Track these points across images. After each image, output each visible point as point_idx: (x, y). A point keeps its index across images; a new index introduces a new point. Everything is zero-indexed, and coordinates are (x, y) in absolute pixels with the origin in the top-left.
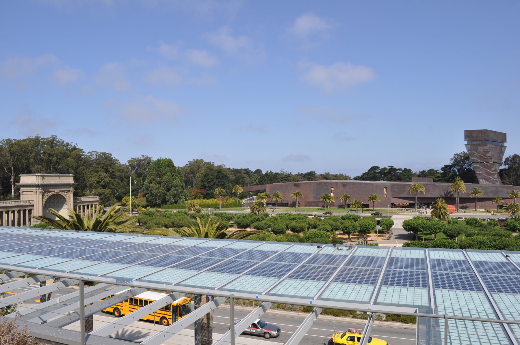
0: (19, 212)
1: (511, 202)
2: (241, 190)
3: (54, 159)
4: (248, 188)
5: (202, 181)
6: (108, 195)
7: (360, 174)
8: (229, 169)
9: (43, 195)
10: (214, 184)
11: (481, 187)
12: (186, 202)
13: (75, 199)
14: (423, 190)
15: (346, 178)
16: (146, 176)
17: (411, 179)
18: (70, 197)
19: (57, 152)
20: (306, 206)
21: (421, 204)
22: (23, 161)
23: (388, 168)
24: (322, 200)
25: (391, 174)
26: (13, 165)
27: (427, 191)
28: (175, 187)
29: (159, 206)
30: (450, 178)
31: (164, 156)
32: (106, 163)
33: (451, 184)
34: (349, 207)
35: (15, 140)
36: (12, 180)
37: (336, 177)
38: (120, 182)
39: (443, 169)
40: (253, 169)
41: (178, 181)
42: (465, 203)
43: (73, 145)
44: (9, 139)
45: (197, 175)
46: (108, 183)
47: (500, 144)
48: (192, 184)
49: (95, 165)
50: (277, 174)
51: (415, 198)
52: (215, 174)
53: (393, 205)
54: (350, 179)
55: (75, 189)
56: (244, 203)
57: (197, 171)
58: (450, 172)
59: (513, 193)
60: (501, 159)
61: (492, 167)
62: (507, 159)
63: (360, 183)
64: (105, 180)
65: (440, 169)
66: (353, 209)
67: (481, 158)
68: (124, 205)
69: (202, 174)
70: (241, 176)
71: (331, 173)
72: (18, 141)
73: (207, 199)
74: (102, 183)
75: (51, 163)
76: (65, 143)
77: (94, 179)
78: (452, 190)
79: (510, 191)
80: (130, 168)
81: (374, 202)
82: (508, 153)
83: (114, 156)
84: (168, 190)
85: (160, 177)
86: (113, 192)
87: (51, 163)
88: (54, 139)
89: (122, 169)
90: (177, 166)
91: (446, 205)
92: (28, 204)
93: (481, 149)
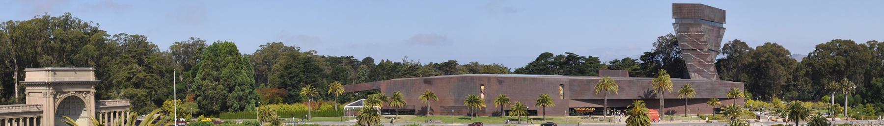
0: (25, 120)
1: (729, 104)
2: (341, 90)
3: (69, 47)
4: (352, 87)
5: (282, 76)
6: (143, 98)
7: (524, 65)
8: (323, 57)
9: (55, 98)
10: (300, 81)
11: (693, 83)
12: (257, 109)
13: (97, 103)
14: (614, 88)
15: (503, 70)
16: (197, 69)
17: (598, 72)
18: (90, 101)
19: (71, 36)
20: (442, 113)
21: (612, 108)
22: (28, 51)
23: (566, 55)
24: (466, 104)
25: (570, 65)
26: (17, 57)
27: (621, 89)
28: (240, 85)
29: (216, 114)
30: (652, 71)
31: (223, 37)
32: (139, 50)
33: (653, 79)
34: (507, 114)
35: (18, 22)
36: (15, 77)
37: (489, 69)
38: (159, 78)
39: (642, 58)
40: (360, 58)
41: (245, 76)
42: (671, 106)
43: (93, 25)
44: (10, 22)
45: (274, 67)
46: (143, 80)
47: (718, 25)
48: (266, 81)
49: (123, 54)
50: (398, 64)
51: (603, 100)
52: (302, 66)
53: (572, 112)
54: (509, 72)
55: (97, 89)
56: (346, 110)
57: (274, 61)
58: (652, 62)
59: (733, 92)
60: (718, 45)
61: (707, 56)
62: (726, 46)
63: (524, 79)
64: (138, 75)
65: (639, 57)
66: (514, 117)
67: (693, 43)
68: (166, 113)
69: (280, 65)
70: (341, 68)
71: (480, 63)
72: (22, 23)
73: (290, 104)
74: (134, 79)
75: (64, 52)
76: (82, 23)
77: (123, 74)
78: (654, 88)
79: (729, 89)
80: (173, 57)
81: (544, 106)
82: (728, 38)
83: (151, 40)
84: (231, 90)
85: (218, 70)
86: (149, 93)
87: (64, 52)
88: (67, 19)
89: (162, 59)
90: (242, 54)
91: (646, 110)
92: (35, 109)
93: (693, 31)
